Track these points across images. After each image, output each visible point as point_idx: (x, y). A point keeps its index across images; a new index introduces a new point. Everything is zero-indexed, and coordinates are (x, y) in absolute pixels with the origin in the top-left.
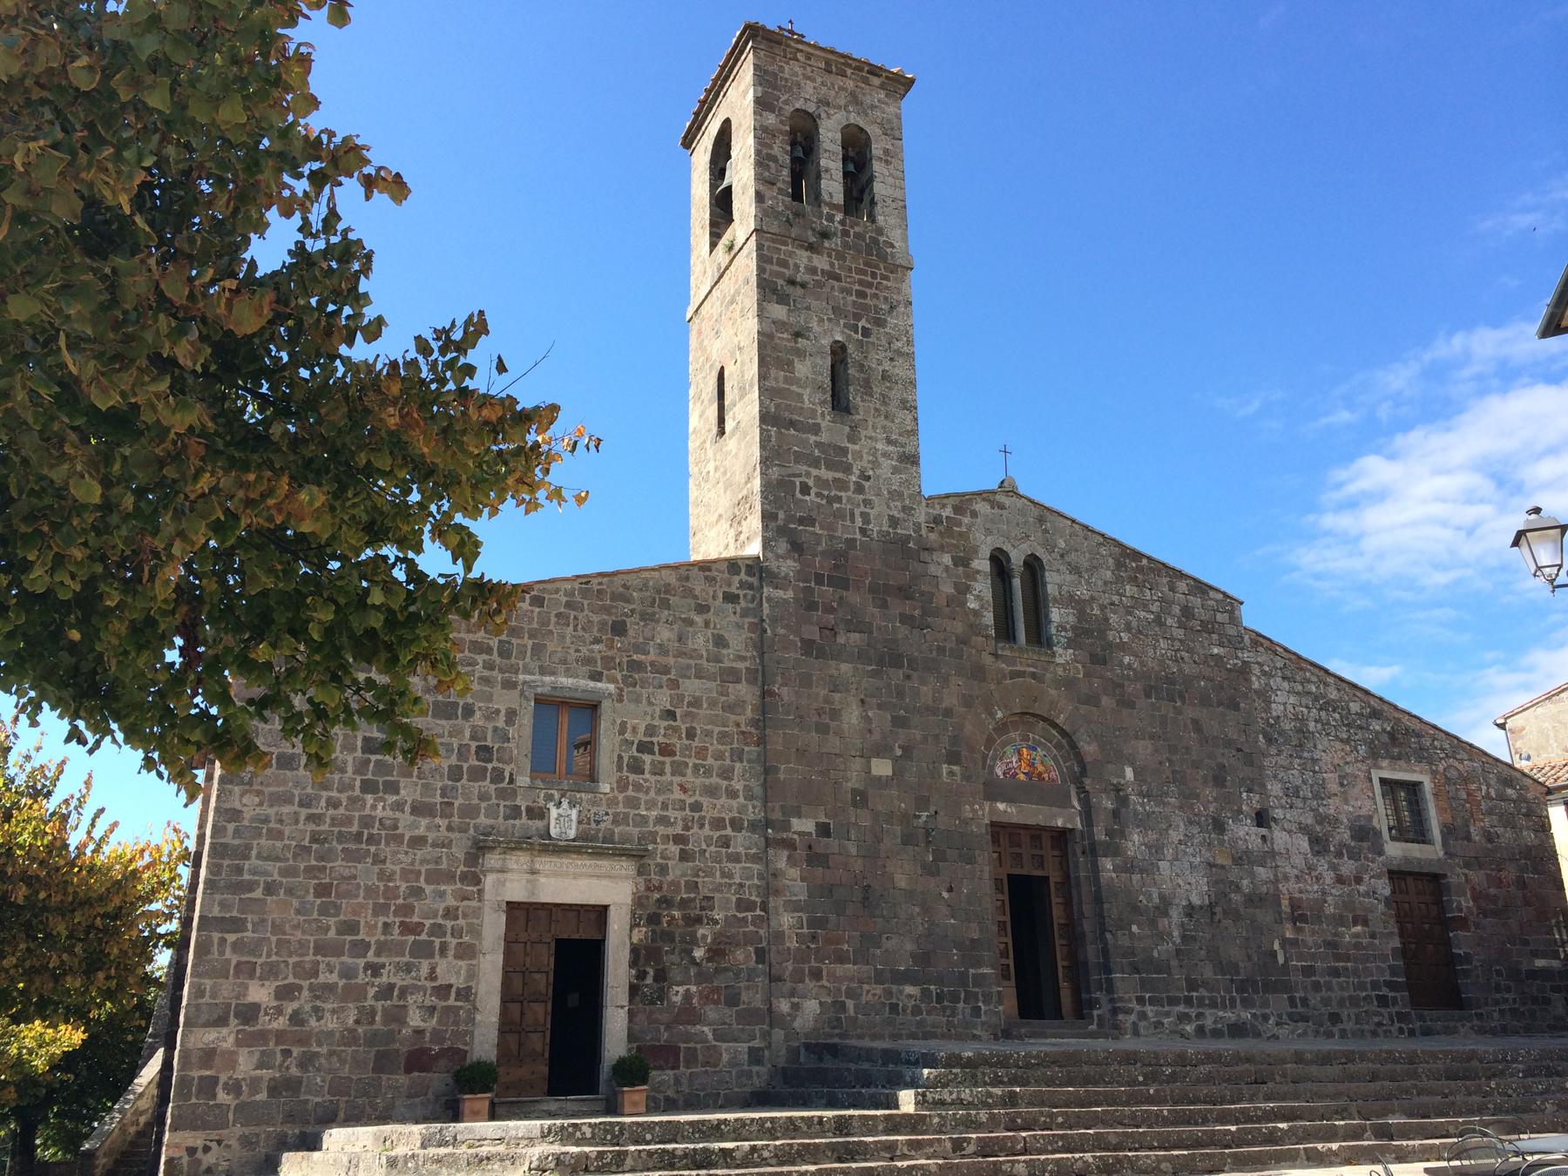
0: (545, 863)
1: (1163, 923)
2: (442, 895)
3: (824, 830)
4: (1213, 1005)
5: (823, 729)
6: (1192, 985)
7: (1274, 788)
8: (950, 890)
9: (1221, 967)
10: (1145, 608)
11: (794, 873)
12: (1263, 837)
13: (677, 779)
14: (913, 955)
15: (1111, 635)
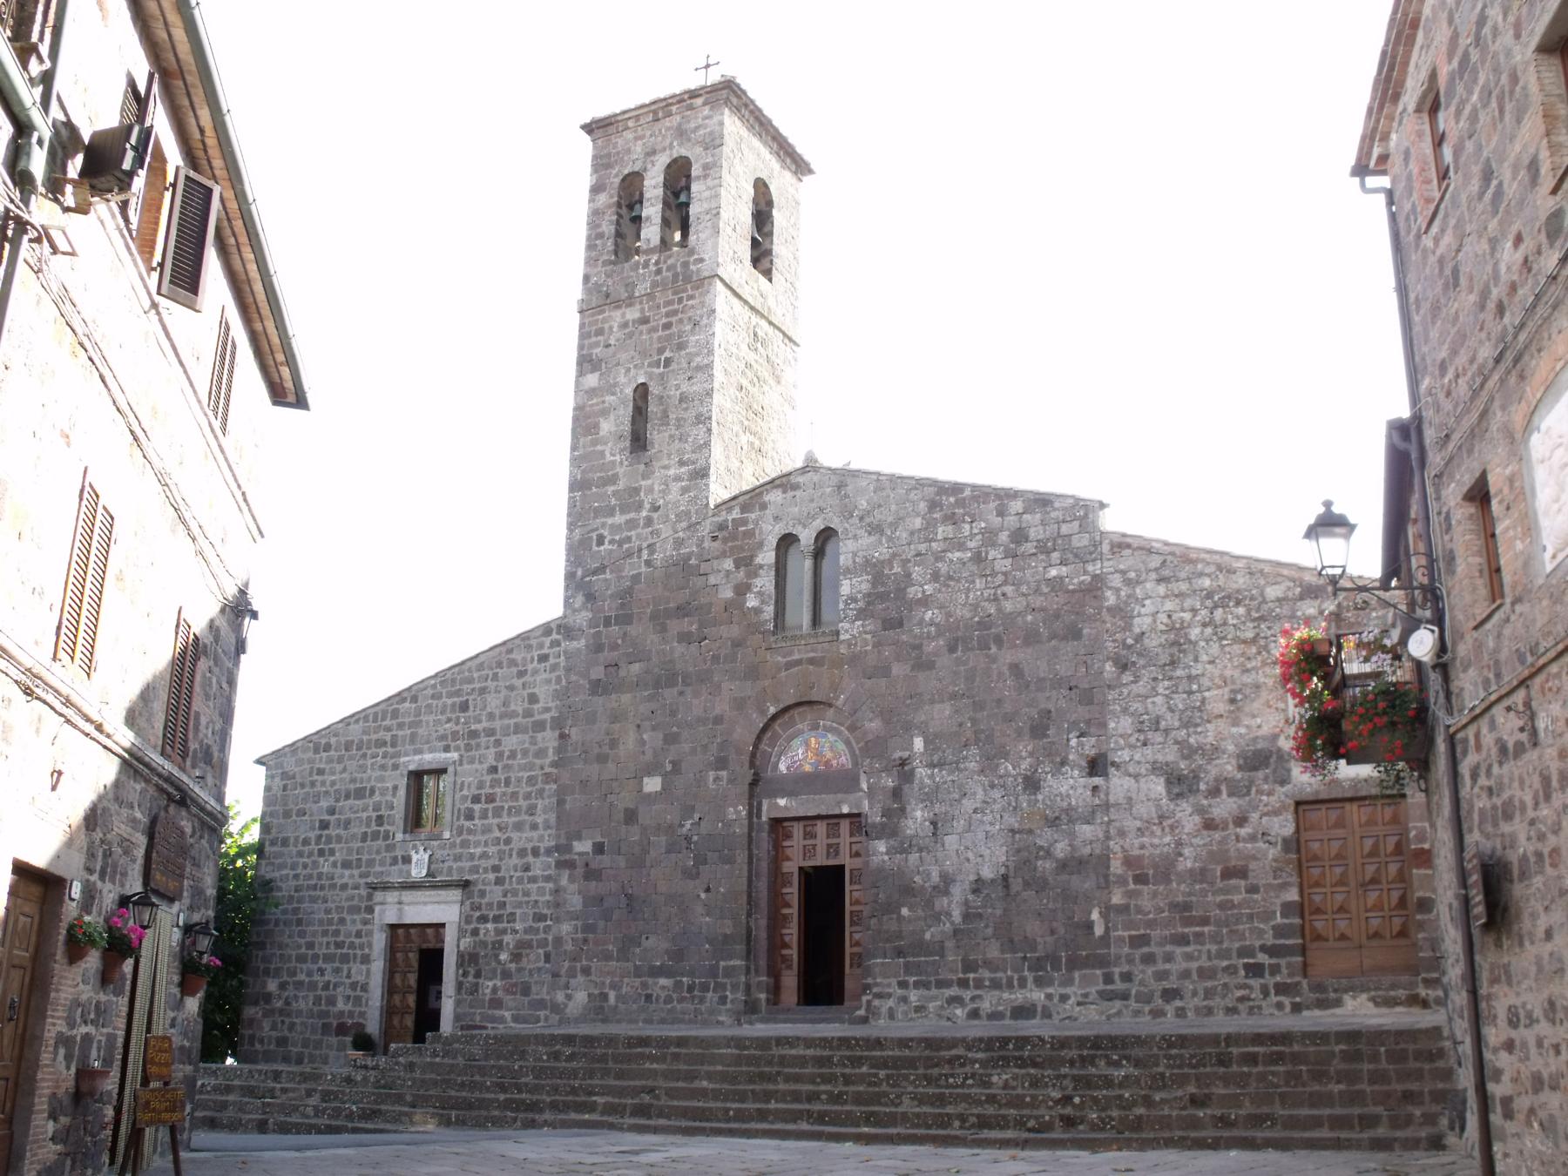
0: (408, 896)
1: (942, 903)
2: (354, 922)
3: (599, 849)
4: (996, 985)
5: (602, 759)
6: (969, 966)
7: (1121, 725)
8: (708, 890)
9: (1010, 945)
10: (961, 547)
11: (574, 887)
12: (1095, 788)
13: (496, 821)
14: (667, 952)
15: (913, 592)
